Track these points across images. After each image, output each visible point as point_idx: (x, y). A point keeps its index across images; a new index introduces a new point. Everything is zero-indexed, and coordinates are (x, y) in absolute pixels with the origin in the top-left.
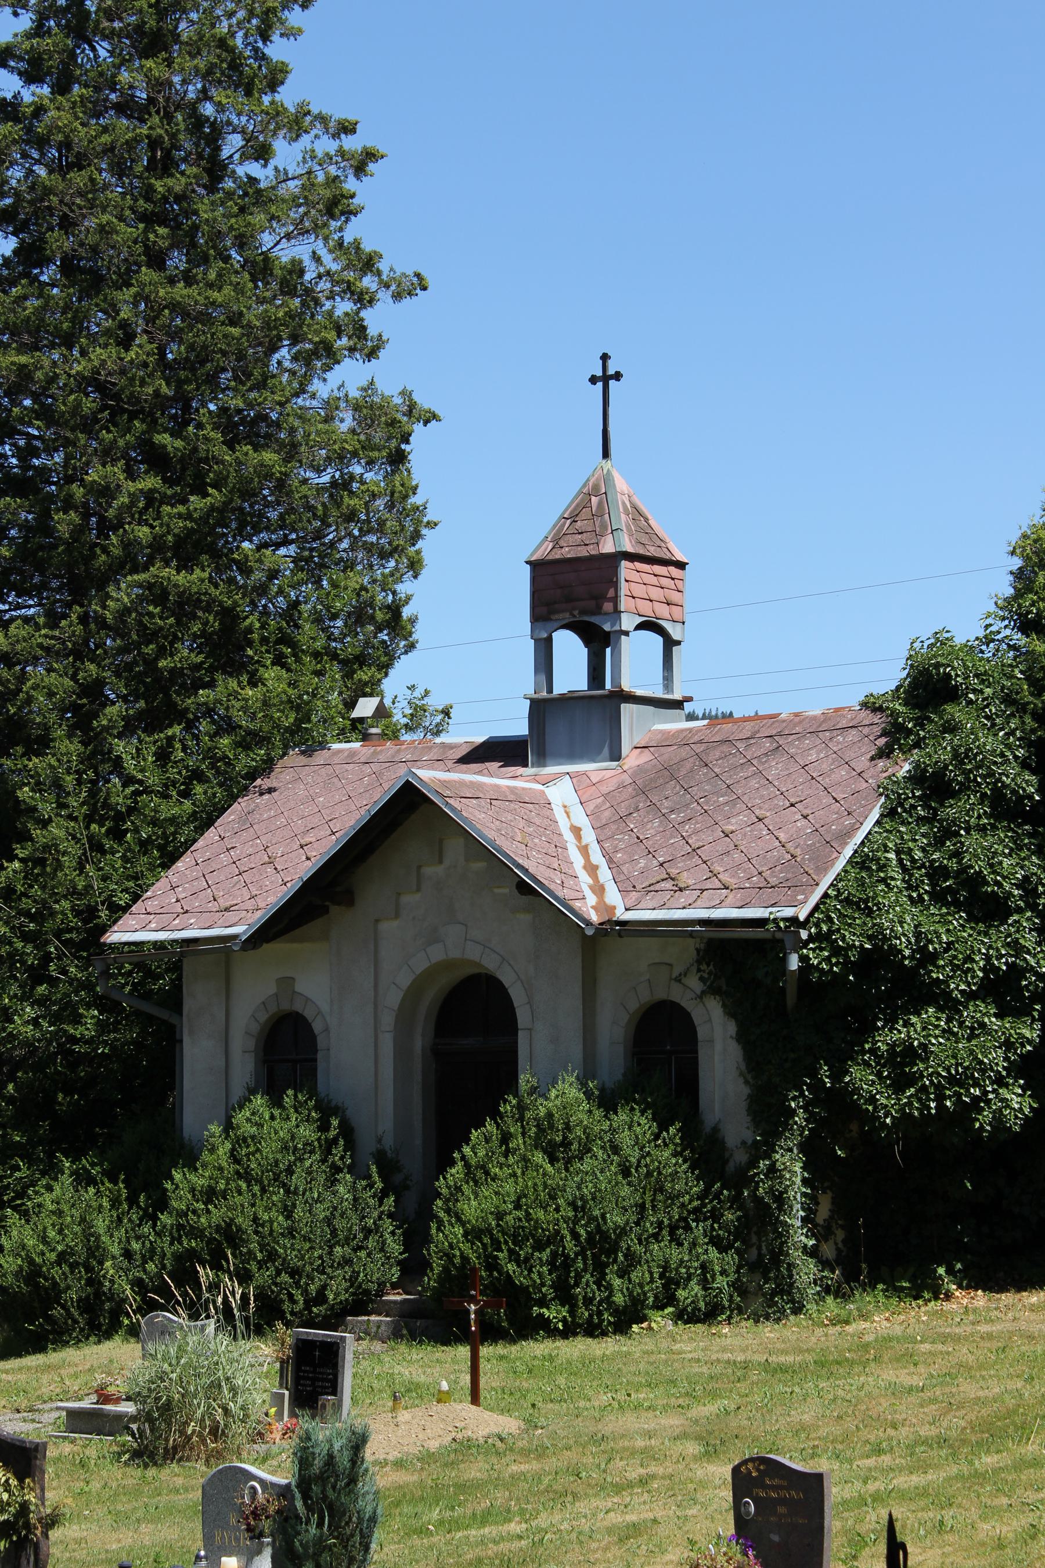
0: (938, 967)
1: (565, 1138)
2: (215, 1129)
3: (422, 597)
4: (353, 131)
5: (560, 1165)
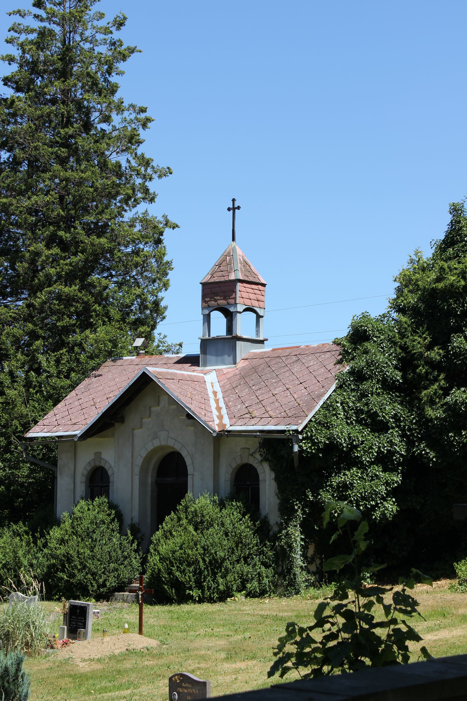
0: (357, 451)
1: (202, 520)
2: (66, 514)
3: (167, 298)
4: (145, 111)
5: (199, 532)
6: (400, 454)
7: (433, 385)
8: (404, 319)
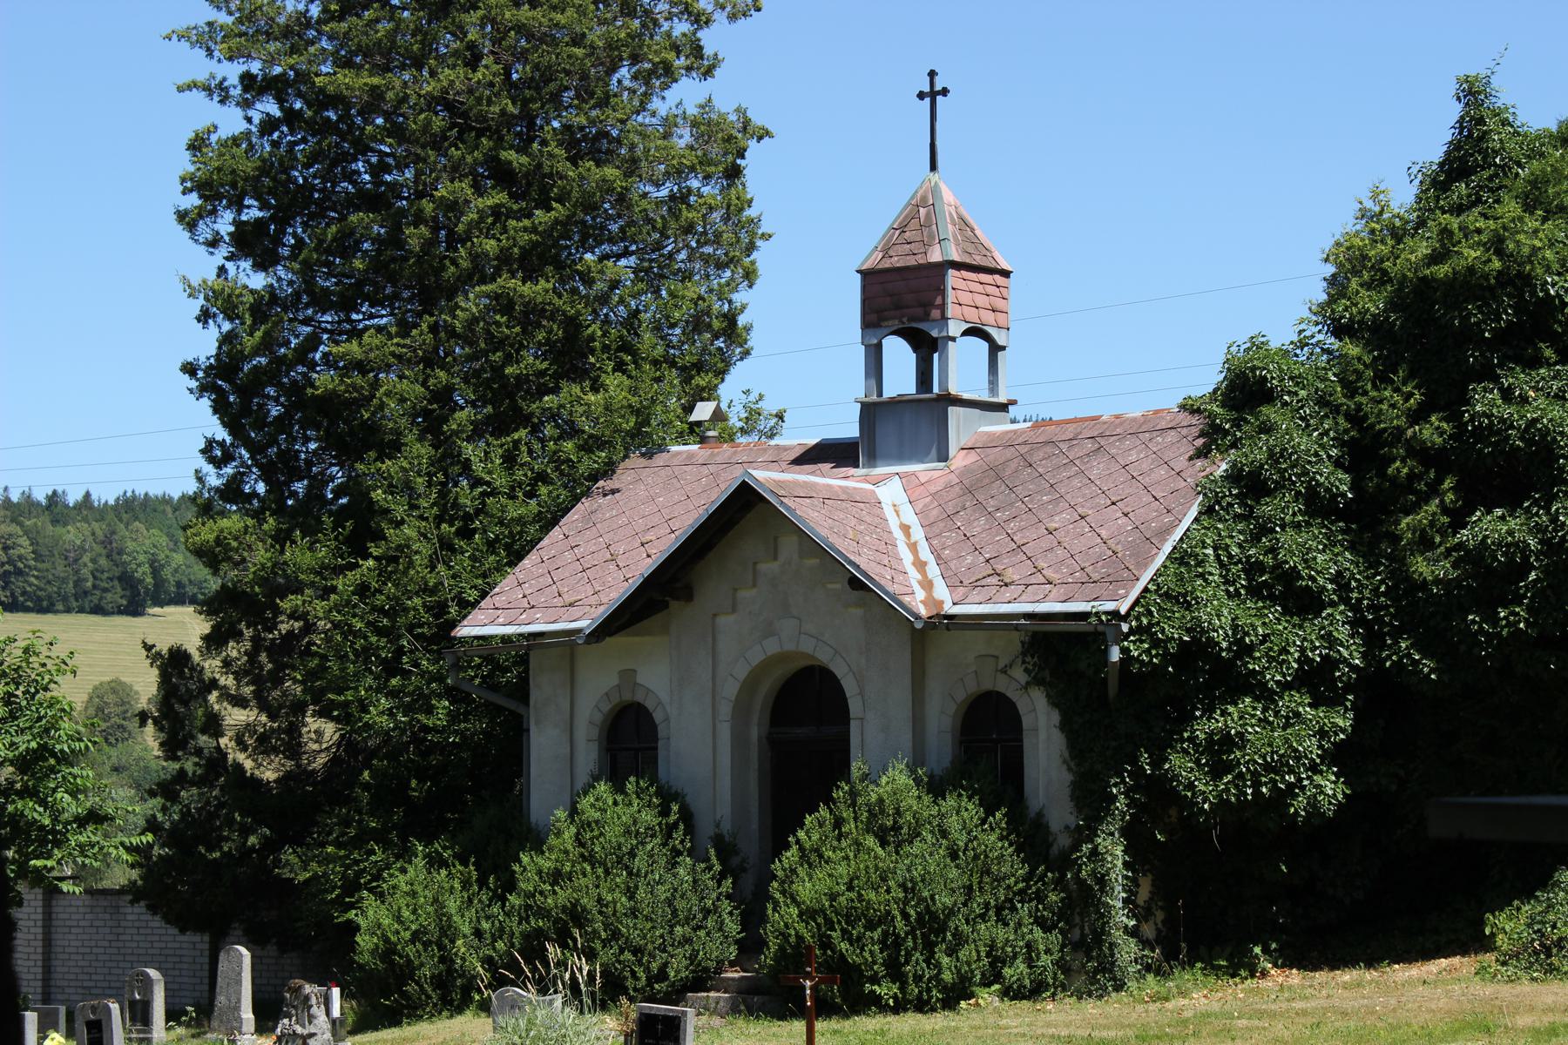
1: (895, 822)
2: (561, 814)
3: (757, 307)
5: (891, 848)
6: (1350, 665)
7: (1427, 503)
8: (1353, 350)
